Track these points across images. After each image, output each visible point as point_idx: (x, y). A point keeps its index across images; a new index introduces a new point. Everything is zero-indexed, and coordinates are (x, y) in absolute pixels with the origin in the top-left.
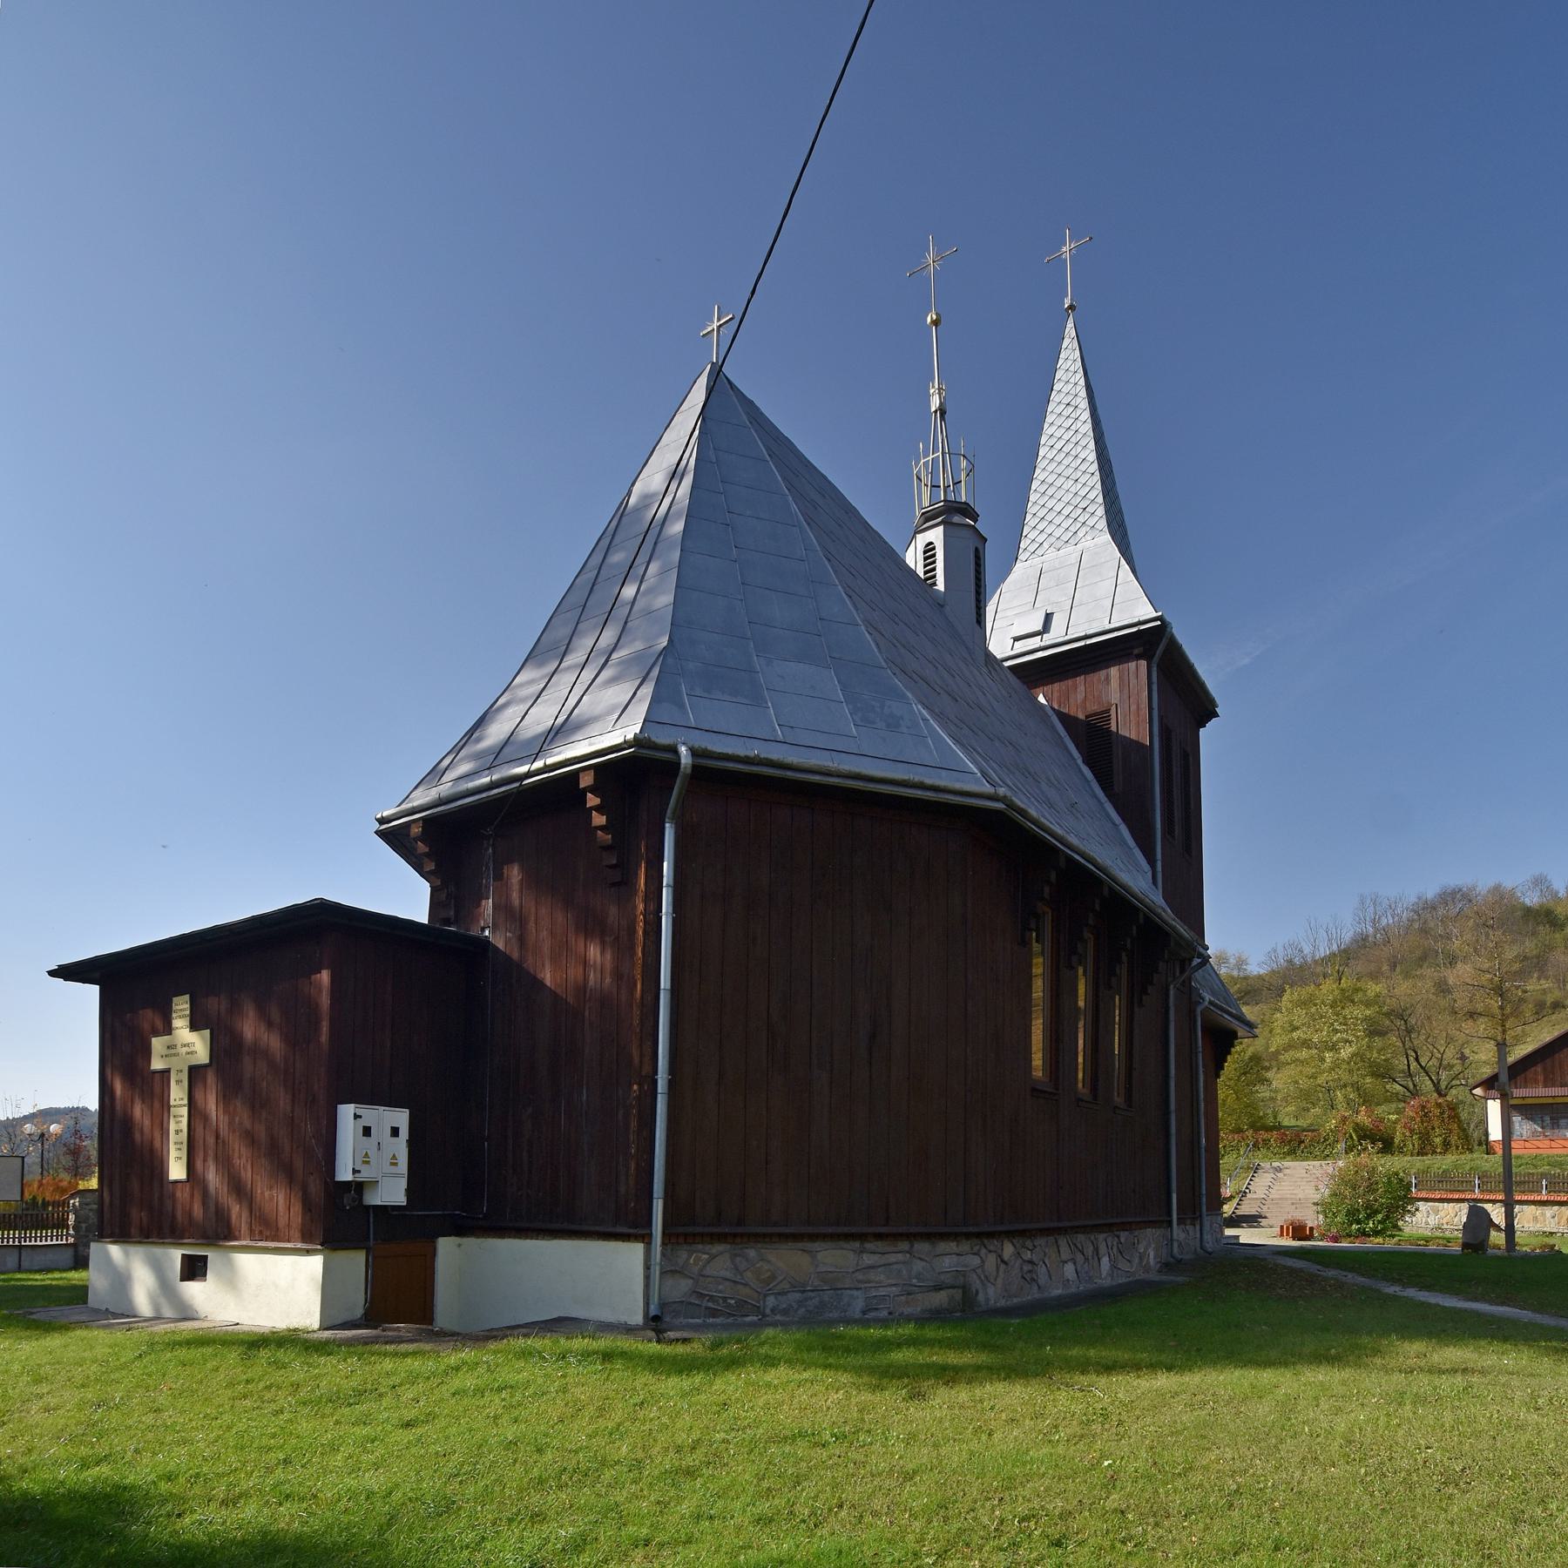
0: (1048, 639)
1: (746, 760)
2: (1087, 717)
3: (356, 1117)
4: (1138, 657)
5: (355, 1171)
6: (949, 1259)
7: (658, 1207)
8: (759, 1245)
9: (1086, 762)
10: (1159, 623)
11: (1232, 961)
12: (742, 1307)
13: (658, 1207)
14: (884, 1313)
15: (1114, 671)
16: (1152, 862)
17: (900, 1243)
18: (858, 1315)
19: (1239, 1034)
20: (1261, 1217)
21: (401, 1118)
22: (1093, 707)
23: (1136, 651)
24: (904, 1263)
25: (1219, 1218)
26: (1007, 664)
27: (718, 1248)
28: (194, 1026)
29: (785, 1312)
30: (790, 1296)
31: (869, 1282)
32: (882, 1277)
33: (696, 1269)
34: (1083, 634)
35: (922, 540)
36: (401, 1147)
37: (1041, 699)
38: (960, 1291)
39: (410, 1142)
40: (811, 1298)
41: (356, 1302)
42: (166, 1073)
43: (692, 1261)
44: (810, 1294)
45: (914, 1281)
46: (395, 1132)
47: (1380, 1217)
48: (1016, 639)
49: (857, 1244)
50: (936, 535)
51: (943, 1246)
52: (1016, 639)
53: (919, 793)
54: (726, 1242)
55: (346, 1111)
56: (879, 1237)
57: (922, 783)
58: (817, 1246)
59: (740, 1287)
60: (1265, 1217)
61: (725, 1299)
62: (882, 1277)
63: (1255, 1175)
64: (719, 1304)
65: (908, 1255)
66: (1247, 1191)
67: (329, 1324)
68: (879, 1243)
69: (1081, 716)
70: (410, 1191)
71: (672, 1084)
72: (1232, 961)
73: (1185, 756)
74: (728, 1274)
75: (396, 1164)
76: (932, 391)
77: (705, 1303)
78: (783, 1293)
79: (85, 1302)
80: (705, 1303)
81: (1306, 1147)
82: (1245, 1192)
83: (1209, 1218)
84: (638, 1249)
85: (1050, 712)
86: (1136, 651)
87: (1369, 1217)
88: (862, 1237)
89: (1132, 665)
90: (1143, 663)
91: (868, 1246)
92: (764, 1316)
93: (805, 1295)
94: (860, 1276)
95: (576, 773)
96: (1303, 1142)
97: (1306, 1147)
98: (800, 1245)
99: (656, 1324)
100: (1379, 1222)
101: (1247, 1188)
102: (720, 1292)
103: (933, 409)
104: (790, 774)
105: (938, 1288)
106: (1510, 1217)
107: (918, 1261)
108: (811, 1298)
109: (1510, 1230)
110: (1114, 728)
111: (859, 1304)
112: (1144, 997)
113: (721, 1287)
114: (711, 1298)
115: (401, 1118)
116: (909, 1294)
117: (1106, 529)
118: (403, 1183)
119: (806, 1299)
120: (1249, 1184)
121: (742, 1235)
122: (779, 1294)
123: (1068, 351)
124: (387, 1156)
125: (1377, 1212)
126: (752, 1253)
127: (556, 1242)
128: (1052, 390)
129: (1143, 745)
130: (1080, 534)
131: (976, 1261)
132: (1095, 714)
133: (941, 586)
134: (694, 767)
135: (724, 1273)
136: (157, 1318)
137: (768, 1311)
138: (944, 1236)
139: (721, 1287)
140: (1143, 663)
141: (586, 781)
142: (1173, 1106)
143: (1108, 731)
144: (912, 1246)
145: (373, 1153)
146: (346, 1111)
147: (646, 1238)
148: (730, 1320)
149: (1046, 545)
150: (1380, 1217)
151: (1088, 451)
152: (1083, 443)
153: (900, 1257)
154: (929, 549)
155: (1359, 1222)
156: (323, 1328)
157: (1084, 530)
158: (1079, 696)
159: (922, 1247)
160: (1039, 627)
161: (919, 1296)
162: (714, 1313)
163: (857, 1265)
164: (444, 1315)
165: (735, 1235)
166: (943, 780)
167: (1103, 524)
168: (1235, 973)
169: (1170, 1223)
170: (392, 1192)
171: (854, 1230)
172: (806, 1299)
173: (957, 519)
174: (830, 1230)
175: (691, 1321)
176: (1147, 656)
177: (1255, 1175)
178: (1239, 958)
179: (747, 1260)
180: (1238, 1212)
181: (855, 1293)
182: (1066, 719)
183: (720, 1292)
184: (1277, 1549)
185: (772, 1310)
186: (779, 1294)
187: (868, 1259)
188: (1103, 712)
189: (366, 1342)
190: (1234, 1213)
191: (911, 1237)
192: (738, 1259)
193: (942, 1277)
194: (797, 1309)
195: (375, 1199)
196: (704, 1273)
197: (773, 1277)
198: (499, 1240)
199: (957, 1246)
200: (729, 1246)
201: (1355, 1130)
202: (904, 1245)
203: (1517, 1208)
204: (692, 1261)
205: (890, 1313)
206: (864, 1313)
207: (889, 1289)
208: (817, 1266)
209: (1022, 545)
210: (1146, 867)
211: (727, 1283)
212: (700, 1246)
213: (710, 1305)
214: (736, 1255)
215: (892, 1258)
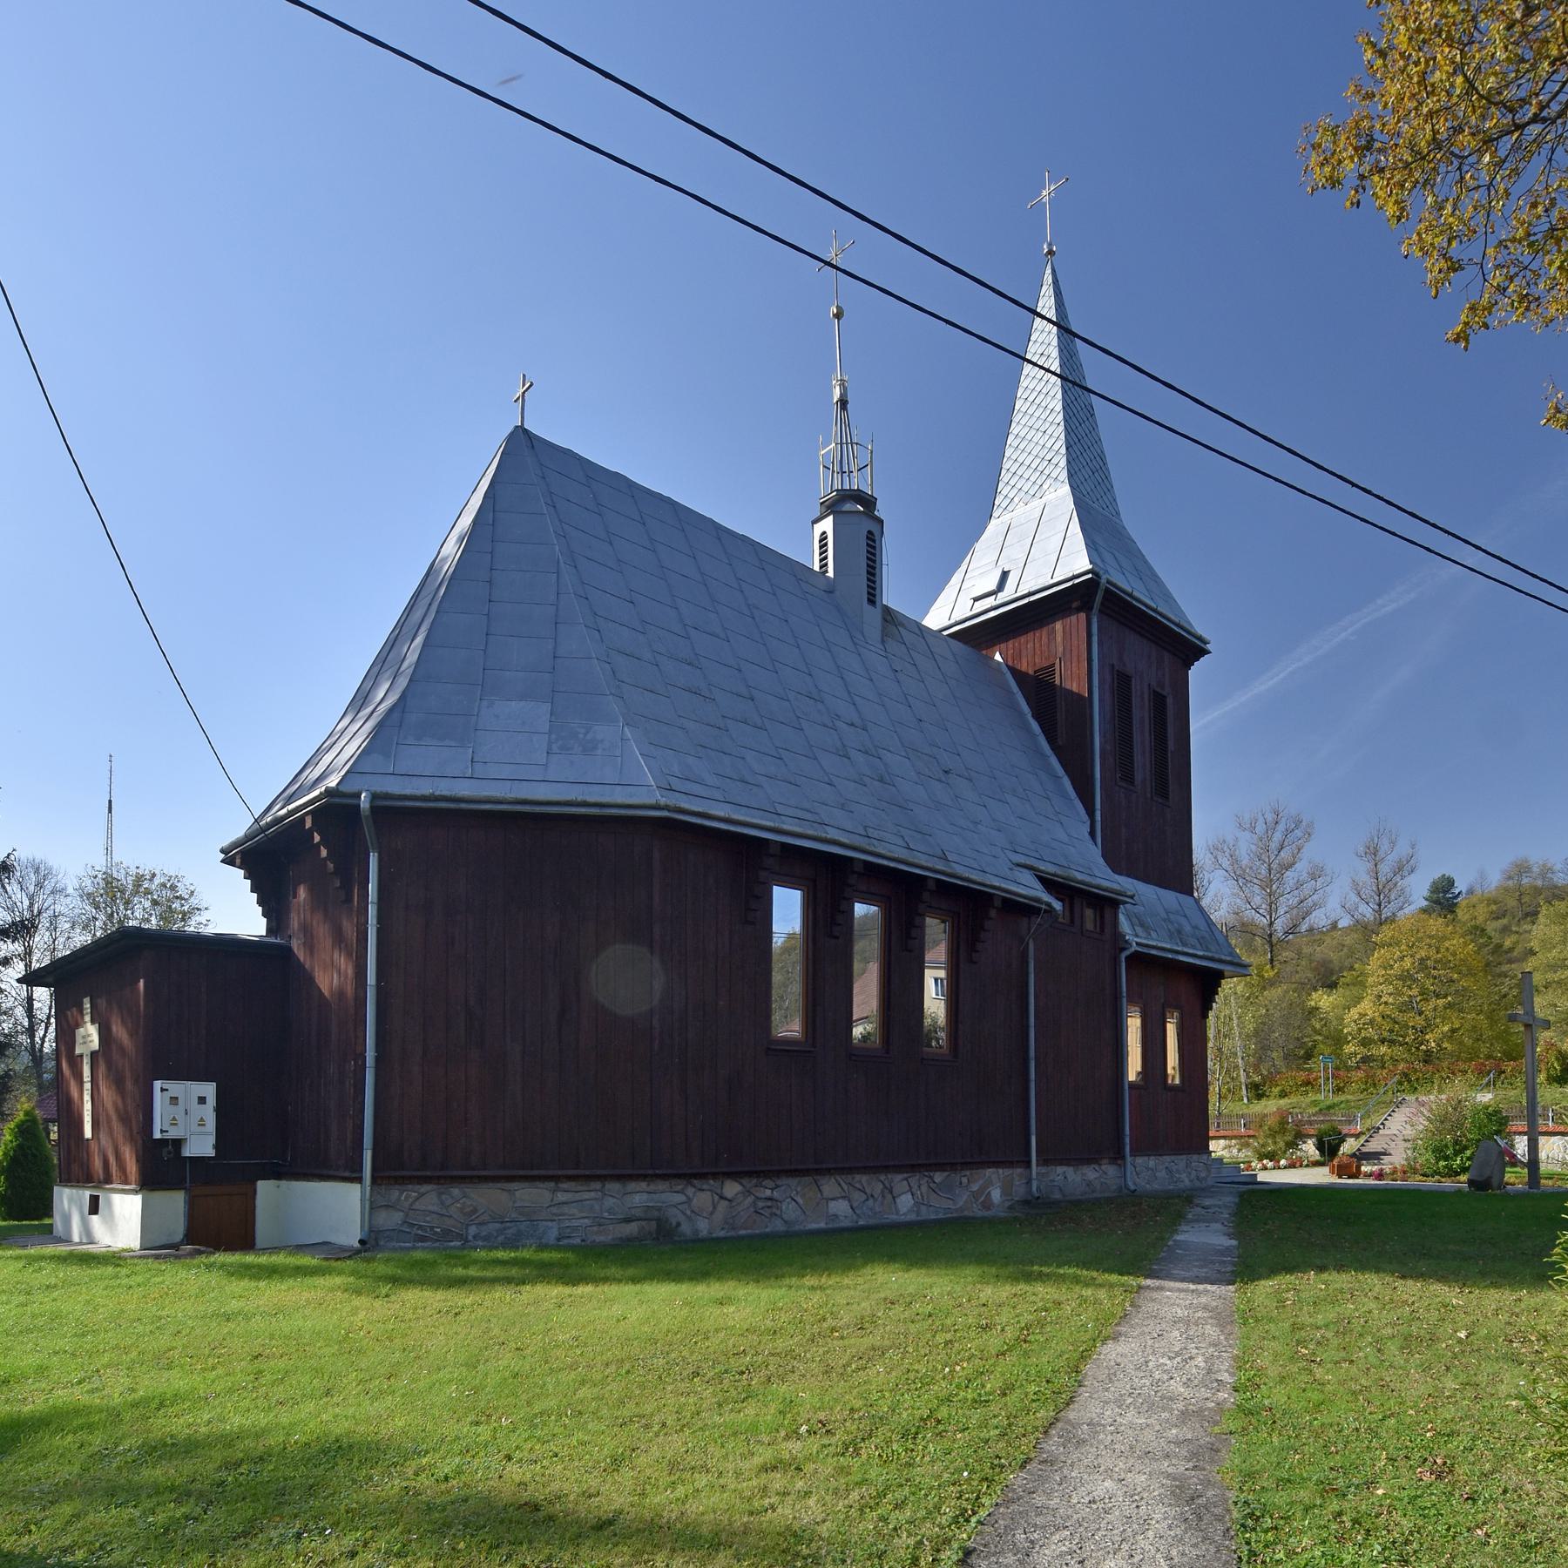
0: (1003, 597)
1: (424, 798)
2: (1035, 672)
3: (162, 1090)
4: (1079, 610)
5: (162, 1131)
6: (639, 1197)
7: (368, 1156)
8: (463, 1186)
9: (1036, 717)
10: (1090, 576)
11: (1536, 870)
12: (447, 1235)
13: (368, 1156)
14: (578, 1241)
15: (1058, 625)
16: (1091, 812)
17: (592, 1183)
18: (552, 1241)
19: (1226, 974)
20: (1385, 1154)
21: (209, 1090)
22: (1041, 662)
23: (1075, 605)
24: (596, 1199)
25: (1205, 1157)
26: (945, 633)
27: (425, 1188)
28: (93, 1022)
29: (486, 1239)
30: (491, 1226)
31: (564, 1215)
32: (575, 1211)
33: (407, 1205)
34: (1071, 575)
35: (819, 528)
36: (209, 1113)
37: (998, 657)
38: (654, 1222)
39: (219, 1110)
40: (509, 1228)
41: (178, 1228)
42: (81, 1056)
43: (403, 1198)
44: (508, 1224)
45: (606, 1214)
46: (202, 1100)
47: (1468, 1153)
48: (976, 599)
49: (552, 1184)
50: (827, 525)
51: (632, 1186)
52: (976, 599)
53: (582, 810)
54: (430, 1183)
55: (158, 1084)
56: (570, 1178)
57: (585, 802)
58: (514, 1186)
59: (446, 1219)
60: (1390, 1154)
61: (432, 1228)
62: (575, 1211)
63: (1396, 1110)
64: (426, 1232)
65: (600, 1193)
66: (1381, 1127)
67: (149, 1246)
68: (573, 1184)
69: (1031, 672)
70: (217, 1147)
71: (379, 1060)
72: (1536, 870)
73: (1159, 702)
74: (435, 1208)
75: (204, 1125)
76: (834, 382)
77: (415, 1231)
78: (482, 1224)
79: (52, 1233)
80: (415, 1231)
81: (1506, 1078)
82: (1379, 1128)
83: (1139, 1160)
84: (356, 1187)
85: (1005, 669)
86: (1075, 605)
87: (1456, 1153)
88: (556, 1179)
89: (1074, 618)
90: (1083, 616)
91: (561, 1185)
92: (467, 1241)
93: (503, 1225)
94: (554, 1210)
95: (302, 819)
96: (1504, 1072)
97: (1506, 1078)
98: (499, 1185)
99: (369, 1244)
100: (1468, 1159)
101: (1382, 1124)
102: (428, 1222)
103: (835, 401)
104: (463, 806)
105: (628, 1220)
106: (1533, 1147)
107: (610, 1198)
108: (509, 1228)
109: (1533, 1164)
110: (1057, 682)
111: (553, 1234)
112: (974, 954)
113: (428, 1219)
114: (420, 1227)
115: (209, 1090)
116: (600, 1225)
117: (1067, 481)
118: (212, 1140)
119: (505, 1229)
120: (1386, 1119)
121: (445, 1177)
122: (480, 1224)
123: (1045, 299)
124: (194, 1120)
125: (1466, 1148)
126: (456, 1192)
127: (323, 1184)
128: (1029, 340)
129: (1083, 697)
130: (1045, 487)
131: (680, 1198)
132: (1042, 669)
133: (831, 574)
134: (372, 807)
135: (431, 1208)
136: (81, 1243)
137: (470, 1238)
138: (631, 1177)
139: (428, 1219)
140: (1083, 616)
141: (308, 824)
142: (1032, 1053)
143: (1053, 684)
144: (604, 1186)
145: (180, 1117)
146: (158, 1084)
147: (359, 1180)
148: (437, 1244)
149: (1016, 500)
150: (1468, 1153)
151: (1056, 401)
152: (1052, 393)
153: (593, 1194)
154: (823, 537)
155: (1446, 1158)
156: (142, 1248)
157: (1048, 482)
158: (1031, 651)
159: (613, 1187)
160: (993, 586)
161: (611, 1227)
162: (423, 1239)
163: (552, 1200)
164: (260, 1240)
165: (439, 1178)
166: (619, 796)
167: (1065, 474)
168: (1539, 883)
169: (1028, 1164)
170: (202, 1145)
171: (551, 1173)
172: (505, 1229)
173: (848, 507)
174: (521, 1173)
175: (402, 1244)
176: (1086, 607)
177: (1396, 1110)
178: (1544, 865)
179: (452, 1197)
180: (1364, 1150)
181: (550, 1224)
182: (1015, 672)
183: (428, 1222)
184: (580, 1413)
185: (474, 1237)
186: (480, 1224)
187: (561, 1197)
188: (1046, 668)
189: (165, 1257)
190: (1359, 1150)
191: (602, 1178)
192: (444, 1197)
193: (633, 1211)
194: (496, 1237)
195: (187, 1152)
196: (414, 1207)
197: (475, 1211)
198: (305, 1183)
199: (648, 1185)
200: (435, 1187)
201: (1557, 1059)
202: (598, 1185)
203: (1542, 1140)
204: (403, 1198)
205: (583, 1241)
206: (558, 1240)
207: (582, 1221)
208: (514, 1202)
209: (997, 503)
210: (1086, 818)
211: (434, 1216)
212: (410, 1187)
213: (420, 1232)
214: (443, 1193)
215: (586, 1195)
